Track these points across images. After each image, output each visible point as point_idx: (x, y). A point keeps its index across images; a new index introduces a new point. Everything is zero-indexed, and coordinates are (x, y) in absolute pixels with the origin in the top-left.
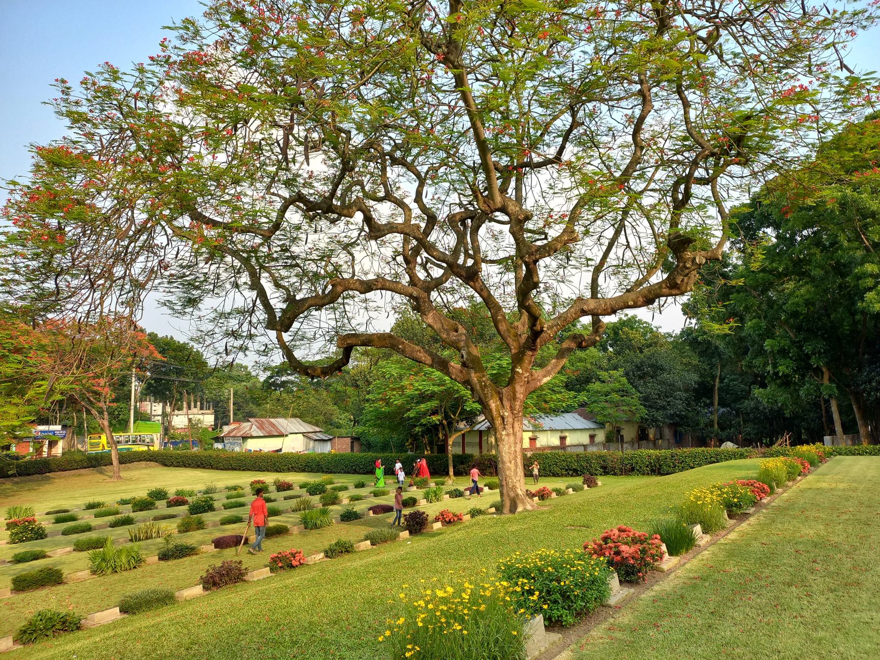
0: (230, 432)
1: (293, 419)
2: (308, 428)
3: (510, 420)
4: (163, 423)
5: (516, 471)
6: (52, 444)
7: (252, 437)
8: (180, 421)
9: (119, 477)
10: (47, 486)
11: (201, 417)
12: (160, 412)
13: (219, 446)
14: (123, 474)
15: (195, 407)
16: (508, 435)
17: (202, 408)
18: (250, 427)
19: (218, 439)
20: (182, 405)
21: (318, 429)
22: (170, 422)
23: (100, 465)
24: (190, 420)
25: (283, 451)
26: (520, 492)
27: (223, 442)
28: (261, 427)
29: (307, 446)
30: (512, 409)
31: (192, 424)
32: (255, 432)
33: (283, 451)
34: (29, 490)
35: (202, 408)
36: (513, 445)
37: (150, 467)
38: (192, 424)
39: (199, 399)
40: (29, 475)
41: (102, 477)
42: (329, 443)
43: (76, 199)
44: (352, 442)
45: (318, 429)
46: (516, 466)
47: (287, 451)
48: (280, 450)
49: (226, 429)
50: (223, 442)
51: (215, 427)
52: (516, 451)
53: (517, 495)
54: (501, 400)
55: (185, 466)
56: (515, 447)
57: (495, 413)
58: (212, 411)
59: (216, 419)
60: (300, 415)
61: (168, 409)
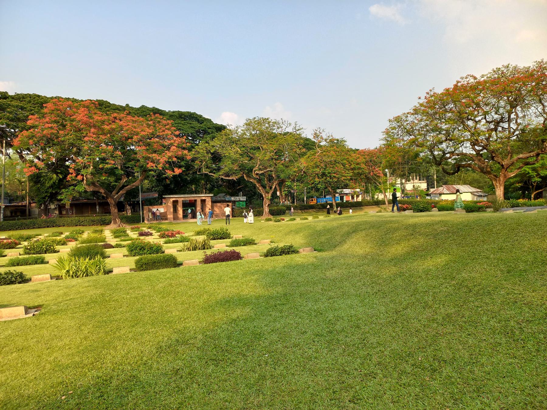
0: (433, 192)
1: (465, 186)
2: (474, 190)
3: (499, 186)
4: (401, 188)
6: (358, 196)
7: (444, 194)
8: (409, 187)
11: (419, 184)
12: (399, 183)
13: (429, 198)
15: (416, 179)
16: (498, 190)
17: (420, 180)
18: (443, 189)
19: (428, 195)
20: (410, 179)
21: (481, 191)
22: (404, 187)
23: (379, 205)
24: (414, 186)
27: (430, 196)
28: (448, 189)
29: (473, 198)
30: (499, 183)
31: (415, 189)
32: (445, 191)
35: (420, 180)
38: (415, 189)
39: (418, 175)
40: (356, 207)
45: (479, 190)
49: (432, 190)
50: (430, 196)
51: (428, 189)
54: (496, 181)
57: (494, 184)
58: (425, 181)
59: (428, 185)
60: (471, 184)
61: (404, 181)
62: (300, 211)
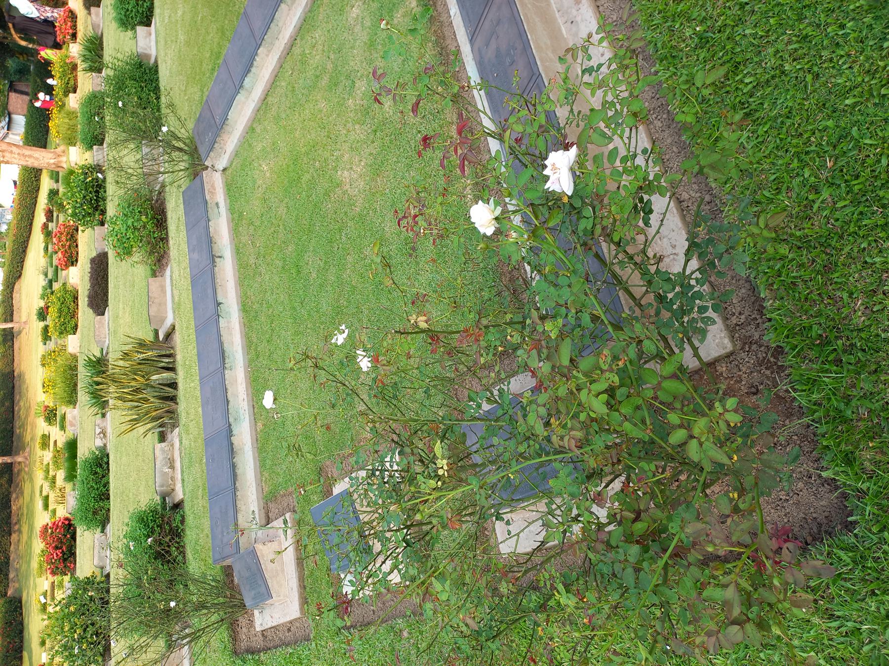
5: (37, 159)
9: (25, 323)
10: (26, 377)
14: (24, 319)
25: (16, 179)
26: (52, 161)
33: (16, 179)
34: (28, 391)
36: (13, 155)
37: (20, 290)
40: (13, 387)
41: (23, 334)
42: (14, 116)
43: (729, 562)
44: (16, 91)
46: (30, 156)
47: (20, 178)
48: (15, 183)
52: (19, 154)
53: (54, 164)
55: (23, 261)
56: (14, 153)
62: (14, 536)
